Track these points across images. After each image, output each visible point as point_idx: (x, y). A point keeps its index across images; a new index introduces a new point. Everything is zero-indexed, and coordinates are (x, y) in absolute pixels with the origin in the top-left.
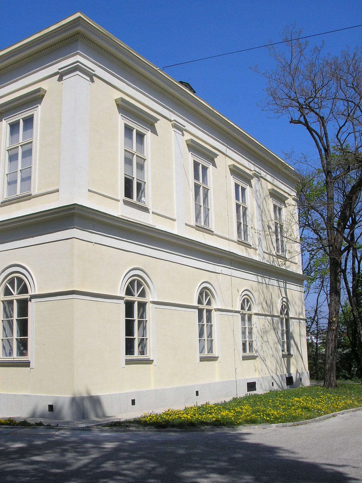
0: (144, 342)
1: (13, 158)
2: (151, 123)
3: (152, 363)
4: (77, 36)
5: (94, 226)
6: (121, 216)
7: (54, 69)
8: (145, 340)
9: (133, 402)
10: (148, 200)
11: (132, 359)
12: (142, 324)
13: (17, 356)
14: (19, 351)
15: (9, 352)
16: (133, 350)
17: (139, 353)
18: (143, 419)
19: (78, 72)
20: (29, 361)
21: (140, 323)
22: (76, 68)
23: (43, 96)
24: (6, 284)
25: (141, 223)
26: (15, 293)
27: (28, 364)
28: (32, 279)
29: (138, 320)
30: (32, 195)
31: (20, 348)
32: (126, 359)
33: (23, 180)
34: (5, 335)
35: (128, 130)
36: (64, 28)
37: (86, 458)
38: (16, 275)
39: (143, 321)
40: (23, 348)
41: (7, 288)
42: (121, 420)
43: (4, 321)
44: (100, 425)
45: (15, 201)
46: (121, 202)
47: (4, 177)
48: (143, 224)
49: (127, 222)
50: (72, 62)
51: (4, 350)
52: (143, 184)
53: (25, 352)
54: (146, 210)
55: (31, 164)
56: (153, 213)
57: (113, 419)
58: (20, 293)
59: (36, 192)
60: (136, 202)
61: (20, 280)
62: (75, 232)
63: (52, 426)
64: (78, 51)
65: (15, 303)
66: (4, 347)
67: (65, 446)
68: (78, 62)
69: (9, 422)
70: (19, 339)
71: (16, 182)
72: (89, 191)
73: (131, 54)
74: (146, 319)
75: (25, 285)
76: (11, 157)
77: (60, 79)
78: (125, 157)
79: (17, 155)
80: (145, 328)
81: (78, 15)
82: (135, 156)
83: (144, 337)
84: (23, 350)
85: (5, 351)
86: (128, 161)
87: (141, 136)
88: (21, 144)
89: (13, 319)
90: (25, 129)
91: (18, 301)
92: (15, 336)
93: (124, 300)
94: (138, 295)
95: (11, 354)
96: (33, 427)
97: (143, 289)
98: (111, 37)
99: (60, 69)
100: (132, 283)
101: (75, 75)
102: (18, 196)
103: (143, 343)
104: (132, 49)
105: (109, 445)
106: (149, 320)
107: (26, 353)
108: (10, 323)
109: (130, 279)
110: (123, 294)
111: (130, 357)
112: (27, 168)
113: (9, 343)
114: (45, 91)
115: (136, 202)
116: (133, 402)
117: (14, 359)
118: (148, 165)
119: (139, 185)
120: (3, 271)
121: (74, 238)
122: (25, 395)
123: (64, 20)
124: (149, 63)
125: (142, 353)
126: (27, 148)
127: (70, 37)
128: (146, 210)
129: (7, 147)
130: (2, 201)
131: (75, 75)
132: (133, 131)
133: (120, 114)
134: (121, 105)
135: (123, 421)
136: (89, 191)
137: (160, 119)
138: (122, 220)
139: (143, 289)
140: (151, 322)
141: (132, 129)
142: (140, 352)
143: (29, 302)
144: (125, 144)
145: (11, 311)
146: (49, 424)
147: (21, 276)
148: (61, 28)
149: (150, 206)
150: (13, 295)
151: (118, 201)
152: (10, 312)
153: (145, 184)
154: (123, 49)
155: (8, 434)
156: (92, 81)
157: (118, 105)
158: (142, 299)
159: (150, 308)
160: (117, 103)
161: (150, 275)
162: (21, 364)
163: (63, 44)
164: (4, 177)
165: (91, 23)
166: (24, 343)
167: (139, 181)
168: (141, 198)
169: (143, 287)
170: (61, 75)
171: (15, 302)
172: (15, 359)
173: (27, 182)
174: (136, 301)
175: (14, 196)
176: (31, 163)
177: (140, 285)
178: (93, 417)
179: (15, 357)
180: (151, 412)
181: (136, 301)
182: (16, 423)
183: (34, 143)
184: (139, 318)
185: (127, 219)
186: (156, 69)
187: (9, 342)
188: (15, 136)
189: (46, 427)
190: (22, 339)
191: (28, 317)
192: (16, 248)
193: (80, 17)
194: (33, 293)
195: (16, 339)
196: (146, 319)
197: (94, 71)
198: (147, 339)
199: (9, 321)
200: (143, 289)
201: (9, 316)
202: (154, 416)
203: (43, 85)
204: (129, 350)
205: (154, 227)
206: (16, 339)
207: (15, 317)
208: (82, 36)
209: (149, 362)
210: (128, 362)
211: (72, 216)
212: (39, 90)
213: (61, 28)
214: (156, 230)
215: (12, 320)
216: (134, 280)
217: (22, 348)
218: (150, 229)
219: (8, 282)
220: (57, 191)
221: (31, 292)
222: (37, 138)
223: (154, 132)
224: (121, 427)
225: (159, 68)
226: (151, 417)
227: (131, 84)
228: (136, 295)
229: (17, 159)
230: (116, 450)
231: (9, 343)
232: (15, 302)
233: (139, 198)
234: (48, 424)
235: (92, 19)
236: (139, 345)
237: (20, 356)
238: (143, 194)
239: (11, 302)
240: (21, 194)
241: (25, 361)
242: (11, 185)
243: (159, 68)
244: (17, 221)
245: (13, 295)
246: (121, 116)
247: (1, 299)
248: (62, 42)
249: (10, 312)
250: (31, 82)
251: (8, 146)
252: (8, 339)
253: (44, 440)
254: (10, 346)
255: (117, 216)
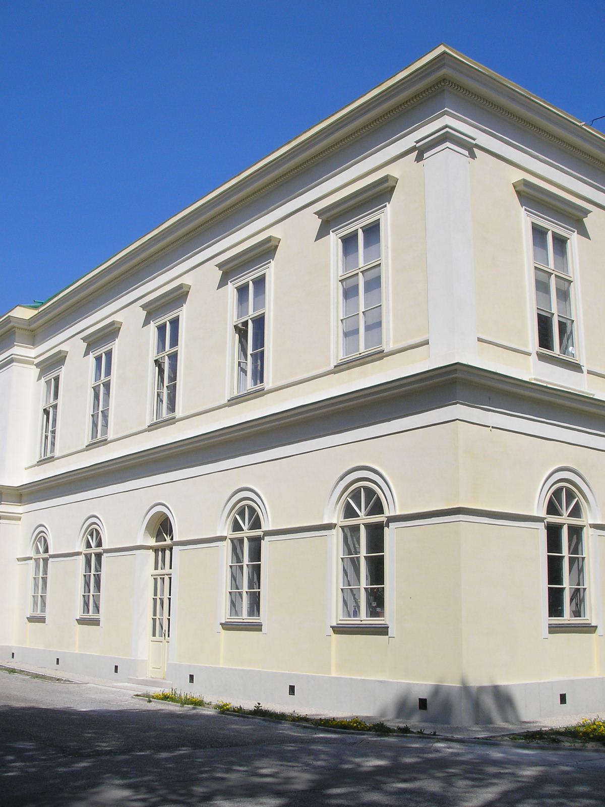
0: (580, 595)
1: (350, 293)
2: (577, 218)
3: (594, 632)
4: (443, 84)
5: (490, 399)
6: (535, 379)
7: (409, 141)
8: (582, 591)
9: (563, 699)
10: (580, 351)
11: (560, 624)
12: (577, 564)
13: (367, 617)
14: (370, 609)
15: (353, 609)
16: (560, 608)
17: (572, 614)
18: (582, 729)
19: (448, 144)
20: (386, 626)
21: (572, 561)
22: (444, 137)
23: (393, 188)
24: (348, 498)
25: (570, 391)
26: (362, 513)
27: (385, 630)
28: (390, 490)
29: (570, 557)
30: (384, 352)
31: (371, 604)
32: (549, 624)
33: (368, 328)
34: (346, 582)
35: (539, 233)
36: (420, 73)
37: (487, 790)
38: (362, 484)
39: (578, 558)
40: (375, 603)
41: (348, 506)
42: (543, 729)
43: (345, 560)
44: (514, 737)
45: (358, 362)
46: (534, 356)
47: (337, 324)
48: (572, 392)
49: (546, 390)
50: (437, 128)
51: (345, 607)
52: (569, 323)
53: (380, 611)
54: (577, 367)
55: (380, 300)
56: (589, 372)
57: (535, 727)
58: (370, 513)
59: (391, 347)
60: (559, 355)
61: (370, 493)
62: (458, 410)
63: (425, 734)
64: (446, 109)
65: (246, 543)
66: (345, 602)
67: (450, 768)
68: (446, 126)
69: (355, 725)
70: (369, 589)
71: (357, 331)
72: (479, 340)
73: (534, 104)
74: (582, 555)
75: (378, 499)
76: (346, 292)
77: (419, 158)
78: (536, 279)
79: (356, 287)
80: (581, 571)
81: (441, 49)
82: (553, 276)
83: (579, 586)
84: (376, 607)
85: (347, 608)
86: (542, 287)
87: (561, 243)
88: (361, 270)
89: (359, 555)
90: (367, 245)
91: (367, 526)
92: (364, 583)
93: (544, 522)
94: (569, 512)
95: (356, 613)
96: (394, 734)
97: (577, 504)
98: (502, 82)
99: (417, 142)
100: (557, 493)
101: (444, 150)
102: (361, 355)
103: (578, 596)
104: (535, 96)
105: (529, 772)
106: (589, 556)
107: (380, 612)
108: (355, 563)
109: (554, 486)
110: (542, 513)
111: (556, 620)
112: (374, 308)
113: (354, 595)
114: (396, 180)
115: (559, 355)
116: (563, 699)
117: (361, 621)
118: (576, 291)
119: (562, 327)
120: (342, 478)
121: (457, 419)
122: (381, 682)
123: (419, 61)
124: (567, 115)
125: (577, 613)
126: (371, 274)
127: (434, 86)
128: (577, 367)
129: (340, 275)
130: (335, 364)
131: (444, 150)
132: (546, 234)
133: (524, 207)
134: (524, 192)
135: (545, 730)
136: (479, 340)
137: (591, 210)
138: (538, 388)
139: (577, 503)
140: (591, 560)
141: (546, 231)
142: (573, 612)
143: (386, 529)
144: (535, 257)
145: (356, 543)
146: (421, 730)
147: (372, 486)
148: (416, 73)
149: (582, 360)
150: (359, 516)
151: (529, 354)
152: (354, 545)
153: (572, 324)
154: (522, 97)
155: (355, 743)
156: (473, 156)
157: (518, 193)
158: (574, 521)
159: (590, 536)
160: (517, 189)
161: (587, 479)
162: (372, 629)
163: (441, 87)
164: (337, 324)
165: (462, 59)
166: (377, 595)
167: (562, 320)
168: (567, 348)
169: (576, 500)
170: (421, 151)
171: (362, 528)
172: (363, 622)
173: (375, 331)
174: (565, 524)
175: (355, 355)
176: (381, 299)
177: (570, 496)
178: (499, 723)
179: (364, 618)
180: (596, 718)
181: (565, 524)
182: (366, 727)
183: (383, 267)
184: (570, 553)
185: (545, 385)
186: (579, 124)
187: (354, 594)
188: (351, 257)
189: (416, 735)
190: (375, 588)
191: (383, 552)
192: (367, 438)
193: (444, 53)
194: (392, 514)
195: (365, 588)
196: (582, 555)
197: (474, 139)
198: (585, 589)
199: (352, 560)
200: (577, 504)
201: (353, 551)
202: (601, 724)
203: (392, 171)
204: (555, 608)
205: (591, 396)
206: (365, 588)
207: (363, 552)
208: (451, 83)
209: (589, 629)
210: (553, 629)
211: (453, 383)
212: (386, 179)
213: (416, 73)
214: (596, 402)
215: (358, 558)
216: (561, 489)
217: (374, 604)
218: (586, 400)
219: (350, 496)
220: (426, 343)
221: (389, 512)
222: (387, 257)
223: (583, 232)
224: (544, 740)
225: (584, 123)
226: (595, 726)
227: (538, 154)
228: (565, 513)
229: (357, 294)
230: (540, 781)
231: (354, 595)
232: (362, 528)
233: (564, 349)
234: (420, 731)
235: (466, 54)
236: (571, 600)
237: (371, 617)
238: (569, 340)
239: (355, 529)
240: (347, 356)
241: (380, 626)
242: (350, 337)
243: (584, 123)
244: (386, 389)
245: (359, 516)
246: (525, 210)
247: (340, 523)
248: (419, 97)
249: (354, 545)
250: (367, 170)
251: (340, 273)
252: (350, 589)
253: (418, 757)
254: (356, 601)
255: (529, 381)
